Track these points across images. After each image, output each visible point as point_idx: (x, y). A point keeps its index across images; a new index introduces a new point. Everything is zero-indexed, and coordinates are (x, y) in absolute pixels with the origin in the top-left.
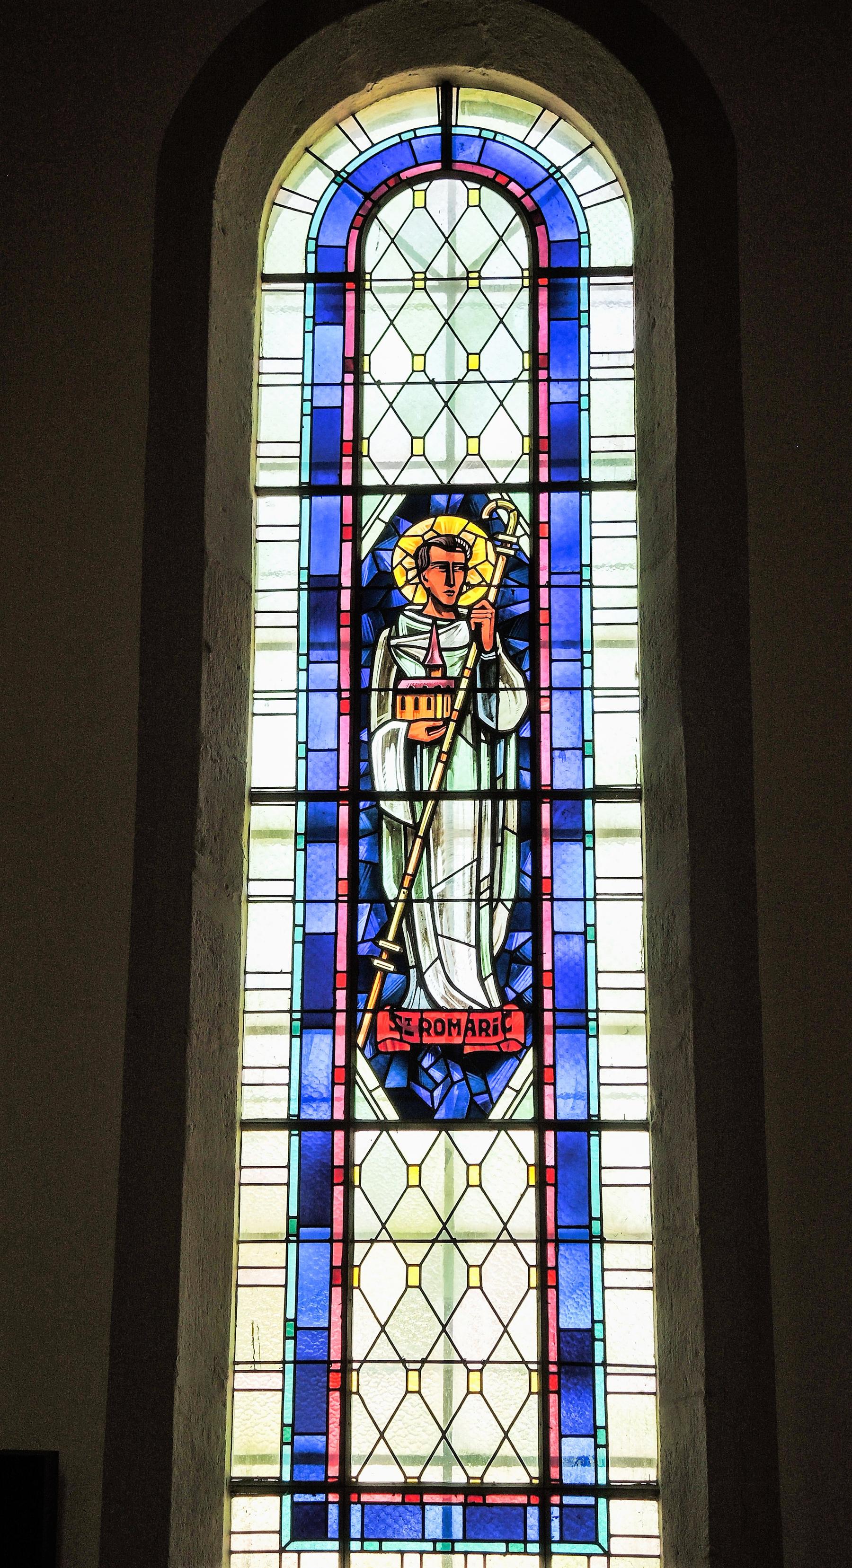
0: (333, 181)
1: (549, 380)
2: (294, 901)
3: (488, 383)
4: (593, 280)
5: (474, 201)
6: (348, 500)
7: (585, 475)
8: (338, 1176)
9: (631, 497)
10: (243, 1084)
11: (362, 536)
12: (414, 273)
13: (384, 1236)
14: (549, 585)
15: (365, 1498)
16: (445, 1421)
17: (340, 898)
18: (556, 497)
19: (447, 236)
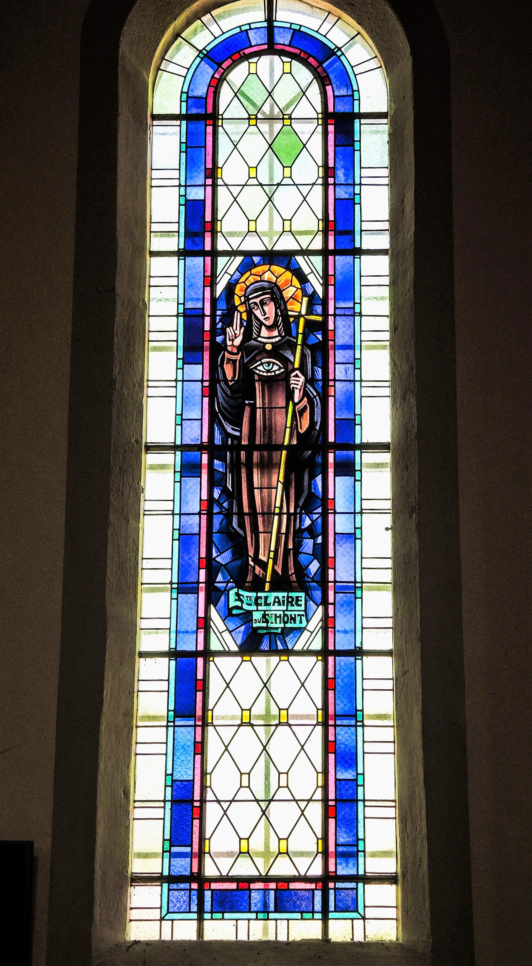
0: (198, 56)
1: (335, 184)
2: (173, 514)
3: (295, 800)
4: (363, 121)
5: (287, 70)
6: (208, 259)
7: (357, 245)
8: (208, 227)
9: (385, 260)
10: (134, 819)
11: (217, 282)
12: (249, 115)
13: (225, 805)
14: (335, 726)
15: (214, 886)
16: (270, 194)
17: (202, 512)
18: (339, 259)
19: (265, 682)
